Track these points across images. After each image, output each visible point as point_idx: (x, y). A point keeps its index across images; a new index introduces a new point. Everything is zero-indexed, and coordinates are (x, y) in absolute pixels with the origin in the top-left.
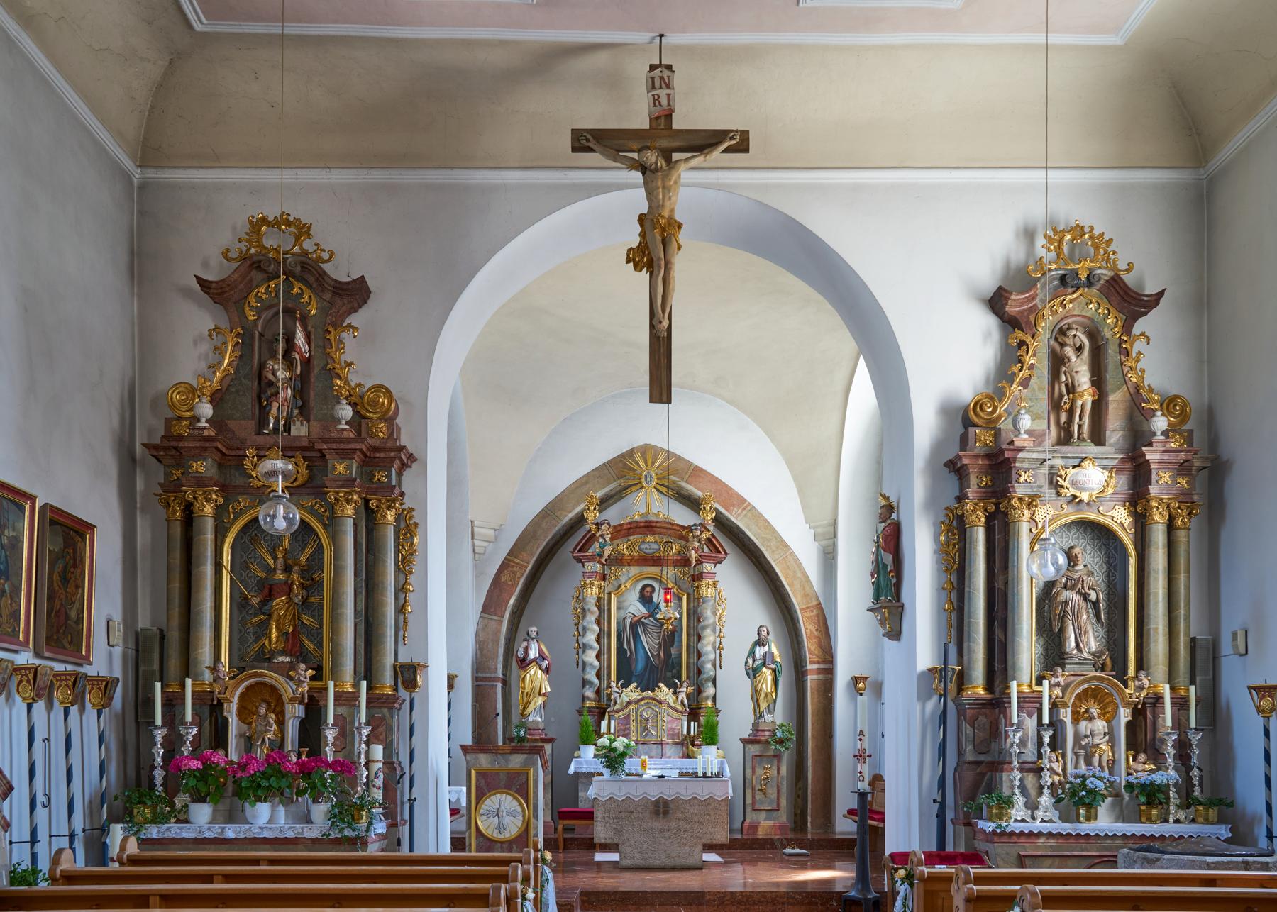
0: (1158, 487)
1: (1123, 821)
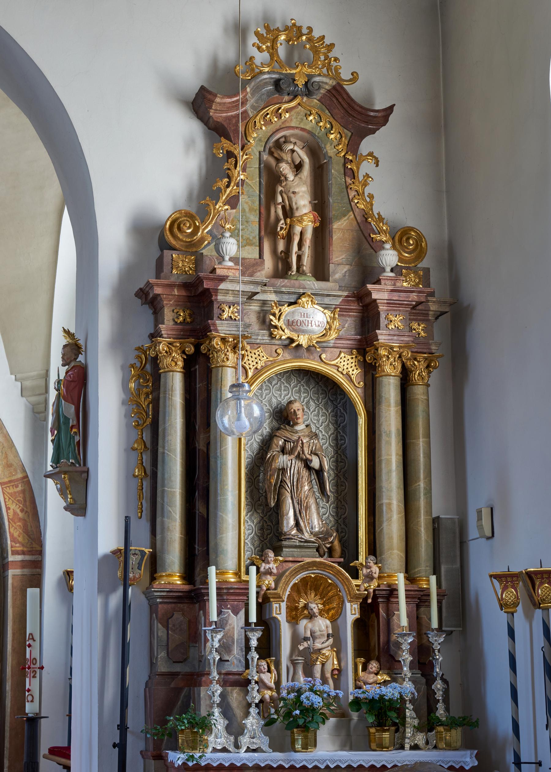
0: (388, 332)
1: (351, 749)
